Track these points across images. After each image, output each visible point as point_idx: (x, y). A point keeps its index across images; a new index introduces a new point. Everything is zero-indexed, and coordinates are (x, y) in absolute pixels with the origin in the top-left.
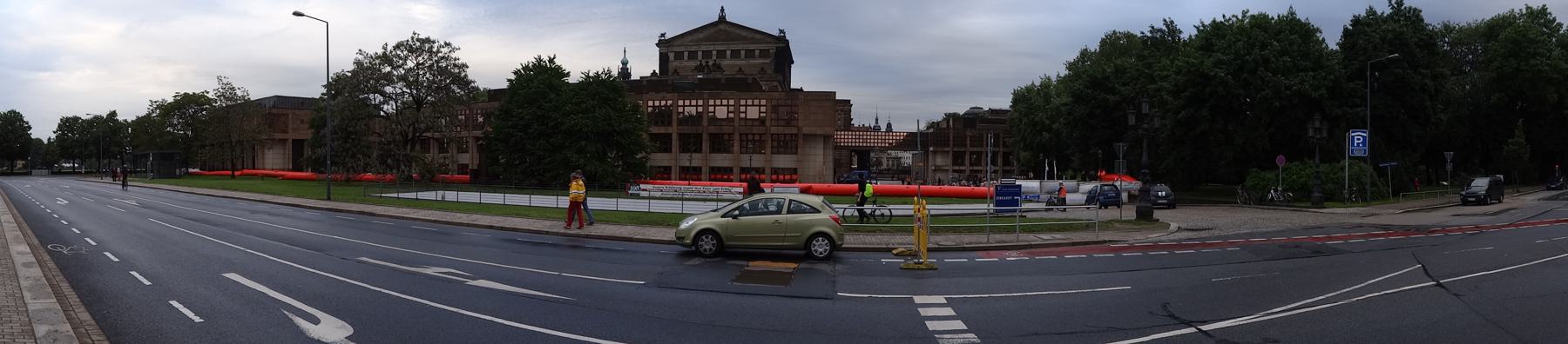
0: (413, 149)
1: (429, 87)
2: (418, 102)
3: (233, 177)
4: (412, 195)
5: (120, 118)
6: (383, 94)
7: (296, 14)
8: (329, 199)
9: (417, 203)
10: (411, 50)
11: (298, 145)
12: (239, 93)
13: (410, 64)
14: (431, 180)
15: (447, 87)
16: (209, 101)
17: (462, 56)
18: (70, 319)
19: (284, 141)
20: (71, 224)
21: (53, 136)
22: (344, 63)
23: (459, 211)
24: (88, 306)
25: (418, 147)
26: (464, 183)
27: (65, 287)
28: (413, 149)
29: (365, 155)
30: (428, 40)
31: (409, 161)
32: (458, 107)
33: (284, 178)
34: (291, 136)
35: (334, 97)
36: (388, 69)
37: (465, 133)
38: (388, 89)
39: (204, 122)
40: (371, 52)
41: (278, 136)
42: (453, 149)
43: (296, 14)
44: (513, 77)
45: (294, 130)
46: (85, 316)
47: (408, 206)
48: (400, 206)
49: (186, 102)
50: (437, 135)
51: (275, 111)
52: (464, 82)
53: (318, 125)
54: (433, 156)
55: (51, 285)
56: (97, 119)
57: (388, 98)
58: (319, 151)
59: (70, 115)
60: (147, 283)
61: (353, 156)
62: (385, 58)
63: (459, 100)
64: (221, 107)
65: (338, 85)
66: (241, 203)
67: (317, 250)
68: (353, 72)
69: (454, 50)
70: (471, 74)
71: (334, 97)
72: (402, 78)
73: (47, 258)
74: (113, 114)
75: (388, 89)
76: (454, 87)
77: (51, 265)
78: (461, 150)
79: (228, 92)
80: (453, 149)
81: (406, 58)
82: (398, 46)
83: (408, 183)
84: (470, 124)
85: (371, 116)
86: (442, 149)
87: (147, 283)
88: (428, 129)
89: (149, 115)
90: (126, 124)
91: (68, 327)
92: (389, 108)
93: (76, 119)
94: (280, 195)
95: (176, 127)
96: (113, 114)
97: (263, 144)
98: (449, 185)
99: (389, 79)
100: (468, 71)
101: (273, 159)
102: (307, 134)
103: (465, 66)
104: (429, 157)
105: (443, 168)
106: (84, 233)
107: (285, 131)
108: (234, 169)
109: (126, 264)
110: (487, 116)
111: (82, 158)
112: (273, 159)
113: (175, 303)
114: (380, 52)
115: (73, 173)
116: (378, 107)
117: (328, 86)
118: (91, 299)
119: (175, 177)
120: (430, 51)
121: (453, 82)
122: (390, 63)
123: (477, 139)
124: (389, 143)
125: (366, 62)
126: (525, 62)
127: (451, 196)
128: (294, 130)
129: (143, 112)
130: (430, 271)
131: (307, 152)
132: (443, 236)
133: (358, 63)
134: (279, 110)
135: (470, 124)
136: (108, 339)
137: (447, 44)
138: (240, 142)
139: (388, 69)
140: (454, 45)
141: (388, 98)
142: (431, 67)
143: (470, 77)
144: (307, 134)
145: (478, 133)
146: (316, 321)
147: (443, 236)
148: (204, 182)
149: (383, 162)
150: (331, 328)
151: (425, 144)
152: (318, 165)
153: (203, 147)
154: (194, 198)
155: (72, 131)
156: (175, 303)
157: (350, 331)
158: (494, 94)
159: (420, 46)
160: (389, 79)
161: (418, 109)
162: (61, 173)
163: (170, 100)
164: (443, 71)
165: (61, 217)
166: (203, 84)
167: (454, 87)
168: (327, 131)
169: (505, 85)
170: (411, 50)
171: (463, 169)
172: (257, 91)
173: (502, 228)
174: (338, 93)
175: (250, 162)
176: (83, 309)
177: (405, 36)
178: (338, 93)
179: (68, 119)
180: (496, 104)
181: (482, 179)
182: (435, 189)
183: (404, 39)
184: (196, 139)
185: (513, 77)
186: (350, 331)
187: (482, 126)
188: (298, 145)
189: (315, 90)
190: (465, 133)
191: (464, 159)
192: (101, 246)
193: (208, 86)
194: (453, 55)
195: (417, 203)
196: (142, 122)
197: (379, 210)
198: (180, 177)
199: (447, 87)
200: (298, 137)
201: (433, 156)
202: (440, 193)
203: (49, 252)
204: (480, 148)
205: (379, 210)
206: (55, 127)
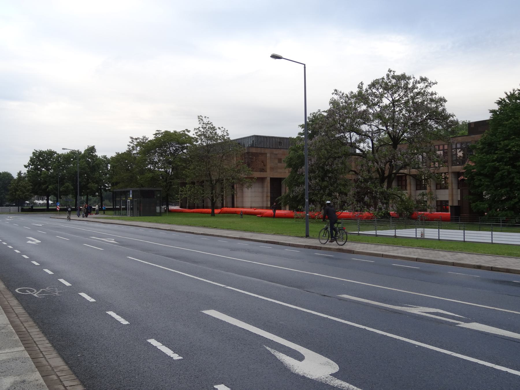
0: (389, 186)
1: (405, 124)
2: (395, 140)
3: (213, 214)
4: (390, 233)
5: (99, 154)
6: (359, 132)
7: (275, 57)
8: (307, 236)
9: (395, 241)
10: (387, 88)
11: (276, 183)
12: (219, 133)
13: (386, 101)
14: (409, 216)
15: (424, 123)
16: (190, 140)
17: (439, 91)
18: (39, 367)
19: (262, 180)
20: (43, 265)
21: (25, 171)
22: (320, 104)
23: (442, 249)
24: (60, 350)
25: (394, 184)
26: (444, 220)
27: (35, 333)
28: (389, 186)
29: (341, 193)
30: (403, 77)
31: (386, 198)
32: (436, 143)
33: (262, 215)
34: (269, 175)
35: (311, 137)
36: (364, 107)
37: (443, 169)
38: (364, 128)
39: (185, 161)
40: (347, 92)
41: (257, 175)
42: (431, 186)
43: (275, 57)
44: (496, 107)
45: (272, 169)
46: (57, 362)
47: (387, 244)
48: (379, 243)
49: (167, 141)
50: (414, 171)
51: (254, 150)
52: (441, 117)
53: (295, 164)
54: (410, 192)
55: (18, 332)
56: (74, 155)
57: (363, 136)
58: (297, 189)
59: (44, 149)
60: (124, 322)
61: (330, 195)
62: (361, 97)
63: (437, 136)
64: (202, 147)
65: (314, 125)
66: (221, 241)
67: (298, 287)
68: (329, 112)
69: (430, 85)
70: (449, 108)
71: (311, 137)
72: (379, 116)
73: (14, 302)
74: (92, 150)
75: (364, 128)
76: (431, 123)
77: (20, 310)
78: (440, 186)
79: (208, 131)
80: (431, 186)
81: (382, 96)
82: (373, 85)
83: (385, 220)
84: (448, 159)
85: (347, 155)
86: (420, 185)
87: (124, 322)
88: (404, 166)
89: (129, 153)
90: (105, 161)
91: (37, 375)
92: (366, 146)
93: (51, 153)
94: (260, 232)
95: (157, 165)
96: (92, 150)
97: (241, 182)
98: (429, 222)
99: (365, 117)
100: (446, 105)
101: (252, 197)
102: (285, 173)
103: (442, 100)
104: (406, 194)
105: (421, 205)
106: (58, 274)
107: (263, 170)
108: (214, 207)
109: (103, 304)
110: (468, 150)
111: (58, 196)
112: (252, 197)
113: (153, 342)
114: (356, 91)
115: (47, 210)
116: (353, 146)
117: (306, 126)
118: (63, 342)
119: (153, 213)
120: (406, 88)
121: (430, 117)
122: (366, 102)
123: (458, 174)
124: (366, 181)
125: (342, 102)
126: (509, 91)
127: (431, 233)
128: (272, 169)
129: (123, 149)
130: (417, 311)
131: (285, 190)
132: (425, 273)
133: (334, 103)
134: (257, 150)
135: (448, 159)
136: (82, 383)
137: (423, 80)
138: (218, 181)
139: (364, 107)
140: (431, 79)
141: (363, 136)
142: (407, 102)
143: (449, 111)
144: (285, 173)
145: (458, 168)
146: (300, 357)
147: (425, 273)
148: (185, 220)
149: (360, 200)
150: (315, 366)
151: (402, 181)
152: (296, 203)
153: (184, 184)
154: (174, 235)
155: (46, 165)
156: (153, 342)
157: (335, 368)
158: (475, 127)
159: (396, 83)
160: (365, 117)
161: (395, 146)
162: (32, 210)
163: (151, 137)
164: (418, 107)
165: (32, 258)
166: (186, 124)
167: (431, 123)
168: (304, 169)
169: (487, 116)
170: (387, 88)
171: (442, 205)
172: (236, 131)
173: (492, 269)
174: (315, 133)
175: (229, 199)
176: (55, 354)
177: (381, 74)
178: (315, 133)
179: (41, 153)
180: (478, 137)
181: (464, 215)
182: (415, 226)
183: (379, 77)
184: (173, 178)
185: (496, 107)
186: (335, 368)
187: (462, 161)
188: (276, 183)
189: (292, 130)
190: (443, 169)
191: (444, 195)
192: (76, 287)
193: (191, 127)
194: (430, 90)
195: (395, 241)
196: (121, 160)
197: (358, 247)
198: (160, 214)
199: (424, 123)
200: (276, 175)
201: (410, 192)
202: (420, 230)
203: (17, 296)
204: (461, 184)
205: (358, 247)
206: (27, 161)
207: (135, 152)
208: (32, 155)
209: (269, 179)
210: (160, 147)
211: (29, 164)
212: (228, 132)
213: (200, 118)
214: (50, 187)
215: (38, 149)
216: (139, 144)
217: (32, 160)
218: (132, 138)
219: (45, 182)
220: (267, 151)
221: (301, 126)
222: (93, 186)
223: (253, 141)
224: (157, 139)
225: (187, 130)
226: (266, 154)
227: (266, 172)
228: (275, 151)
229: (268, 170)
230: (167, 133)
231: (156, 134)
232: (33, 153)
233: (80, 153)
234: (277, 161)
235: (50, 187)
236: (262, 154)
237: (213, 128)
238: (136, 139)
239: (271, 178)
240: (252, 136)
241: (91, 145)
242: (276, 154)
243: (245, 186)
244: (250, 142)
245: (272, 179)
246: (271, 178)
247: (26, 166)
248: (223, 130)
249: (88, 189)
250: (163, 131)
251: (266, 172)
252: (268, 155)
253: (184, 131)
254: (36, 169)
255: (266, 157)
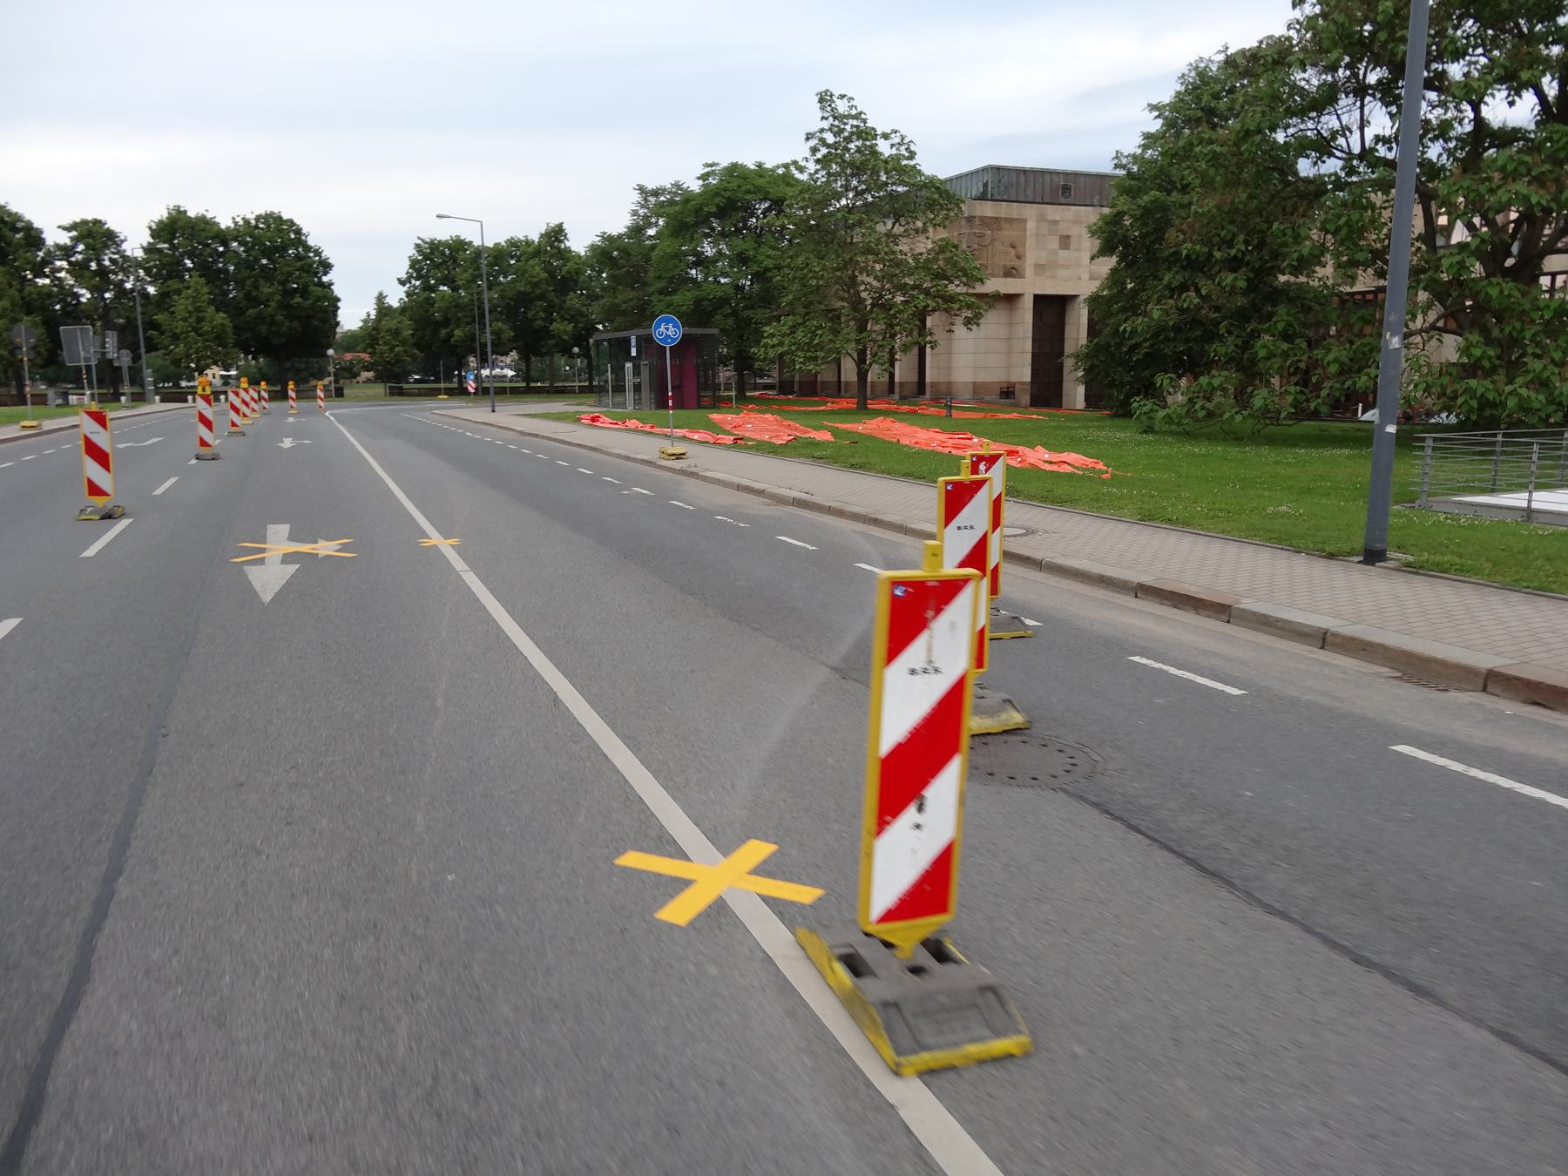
34: (1030, 286)
45: (1040, 268)
56: (516, 249)
74: (556, 234)
96: (556, 234)
107: (1010, 272)
174: (1210, 116)
178: (1210, 116)
206: (403, 269)
207: (651, 232)
208: (413, 252)
209: (1028, 303)
210: (721, 213)
211: (410, 278)
212: (913, 148)
213: (825, 99)
214: (458, 332)
215: (427, 237)
216: (660, 209)
217: (414, 264)
218: (642, 189)
219: (446, 322)
220: (1030, 212)
221: (1153, 107)
222: (562, 328)
223: (985, 185)
224: (709, 193)
225: (795, 163)
226: (1024, 221)
227: (1022, 276)
228: (1053, 212)
229: (1029, 272)
230: (734, 170)
231: (704, 177)
232: (418, 246)
233: (528, 243)
234: (1054, 243)
235: (458, 332)
236: (1010, 220)
237: (866, 134)
238: (656, 193)
239: (1036, 297)
240: (984, 169)
241: (554, 222)
242: (1055, 222)
243: (959, 321)
244: (976, 190)
245: (1038, 299)
246: (1036, 297)
247: (402, 283)
248: (897, 140)
249: (553, 337)
250: (724, 163)
251: (1022, 276)
252: (1031, 225)
253: (786, 166)
254: (428, 288)
255: (1025, 229)
